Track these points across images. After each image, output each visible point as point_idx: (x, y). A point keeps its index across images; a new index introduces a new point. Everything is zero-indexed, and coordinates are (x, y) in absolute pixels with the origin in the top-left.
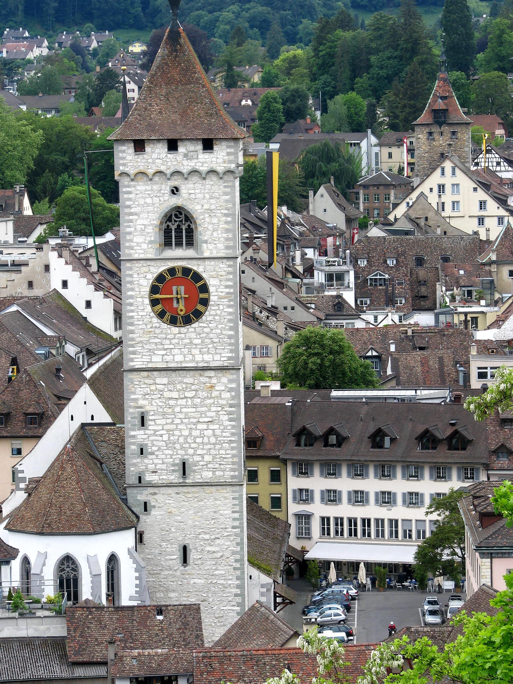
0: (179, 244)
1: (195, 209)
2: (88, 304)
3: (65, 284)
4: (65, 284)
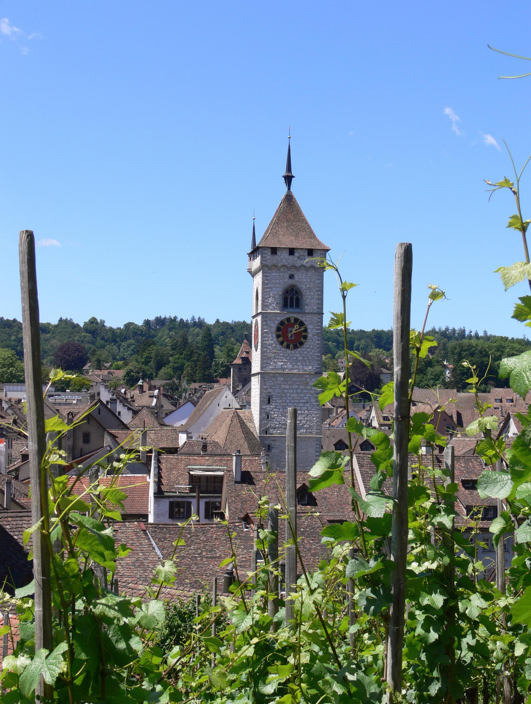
0: (291, 306)
1: (303, 287)
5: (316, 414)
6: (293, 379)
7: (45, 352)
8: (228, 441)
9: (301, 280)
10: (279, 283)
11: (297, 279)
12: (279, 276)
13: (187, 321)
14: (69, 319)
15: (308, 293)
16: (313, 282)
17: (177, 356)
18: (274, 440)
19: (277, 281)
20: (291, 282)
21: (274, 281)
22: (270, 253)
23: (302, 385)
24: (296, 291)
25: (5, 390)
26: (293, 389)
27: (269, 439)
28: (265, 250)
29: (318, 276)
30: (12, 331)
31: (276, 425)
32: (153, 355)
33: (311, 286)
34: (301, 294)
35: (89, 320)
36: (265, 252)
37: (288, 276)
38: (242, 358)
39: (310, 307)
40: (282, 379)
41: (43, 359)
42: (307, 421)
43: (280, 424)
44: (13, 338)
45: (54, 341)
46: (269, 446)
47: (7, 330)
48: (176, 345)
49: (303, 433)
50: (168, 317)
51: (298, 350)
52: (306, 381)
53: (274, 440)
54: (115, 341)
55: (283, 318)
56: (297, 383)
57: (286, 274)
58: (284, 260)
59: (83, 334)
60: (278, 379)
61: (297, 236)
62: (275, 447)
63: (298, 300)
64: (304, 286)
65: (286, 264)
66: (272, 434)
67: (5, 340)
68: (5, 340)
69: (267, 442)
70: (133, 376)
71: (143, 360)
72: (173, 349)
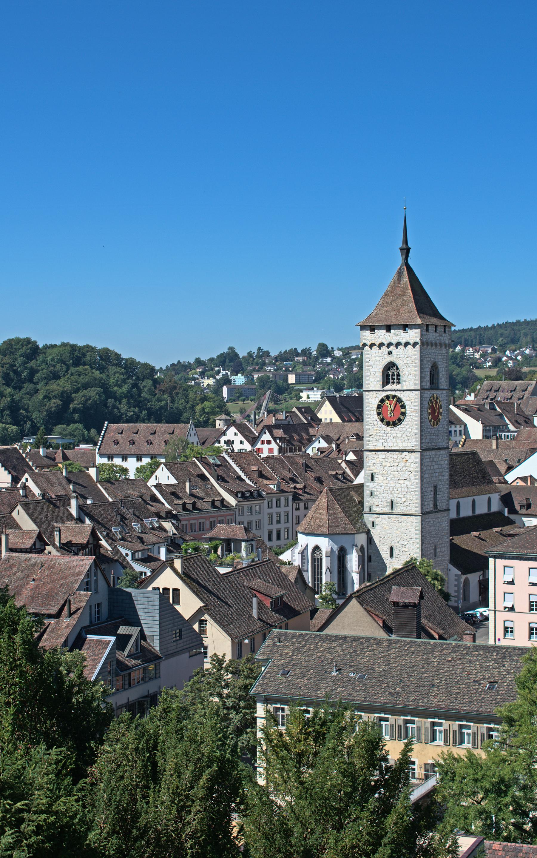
15: (405, 369)
20: (389, 359)
37: (387, 353)
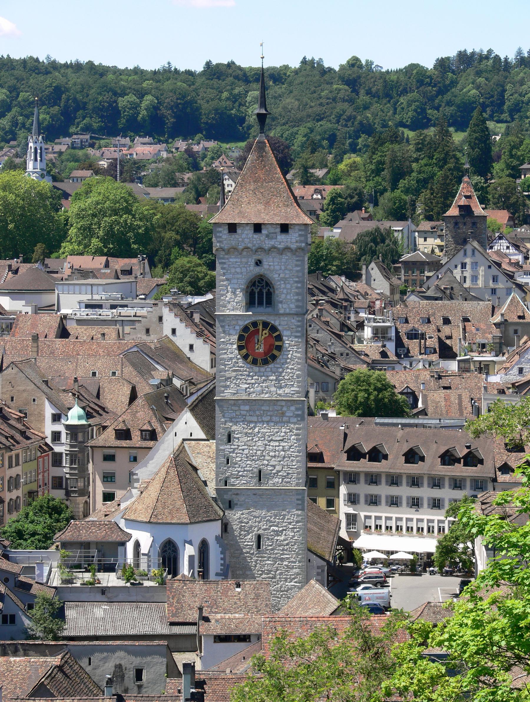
0: (260, 303)
1: (274, 277)
2: (191, 347)
3: (174, 331)
4: (174, 331)
5: (297, 456)
6: (263, 408)
7: (274, 119)
8: (159, 503)
9: (272, 267)
10: (241, 273)
11: (266, 267)
12: (241, 262)
13: (506, 59)
14: (317, 59)
15: (283, 286)
16: (290, 270)
17: (422, 162)
18: (237, 494)
19: (238, 270)
20: (257, 270)
21: (233, 270)
22: (226, 231)
23: (276, 416)
24: (266, 282)
25: (56, 292)
26: (263, 421)
27: (230, 493)
28: (220, 227)
29: (297, 261)
30: (223, 83)
31: (239, 472)
32: (387, 159)
33: (287, 276)
34: (273, 288)
35: (348, 62)
36: (220, 229)
38: (460, 207)
39: (285, 306)
40: (247, 408)
41: (270, 129)
42: (283, 466)
43: (244, 471)
44: (225, 95)
45: (288, 101)
46: (230, 502)
47: (215, 82)
48: (422, 144)
49: (278, 482)
50: (477, 50)
51: (270, 366)
52: (281, 409)
53: (237, 494)
54: (388, 96)
55: (246, 322)
56: (269, 414)
57: (250, 259)
58: (246, 241)
59: (335, 86)
60: (242, 407)
61: (267, 204)
62: (239, 503)
63: (270, 295)
64: (277, 276)
65: (250, 245)
66: (234, 485)
67: (212, 100)
68: (212, 100)
69: (227, 497)
70: (341, 203)
71: (373, 167)
72: (418, 150)
